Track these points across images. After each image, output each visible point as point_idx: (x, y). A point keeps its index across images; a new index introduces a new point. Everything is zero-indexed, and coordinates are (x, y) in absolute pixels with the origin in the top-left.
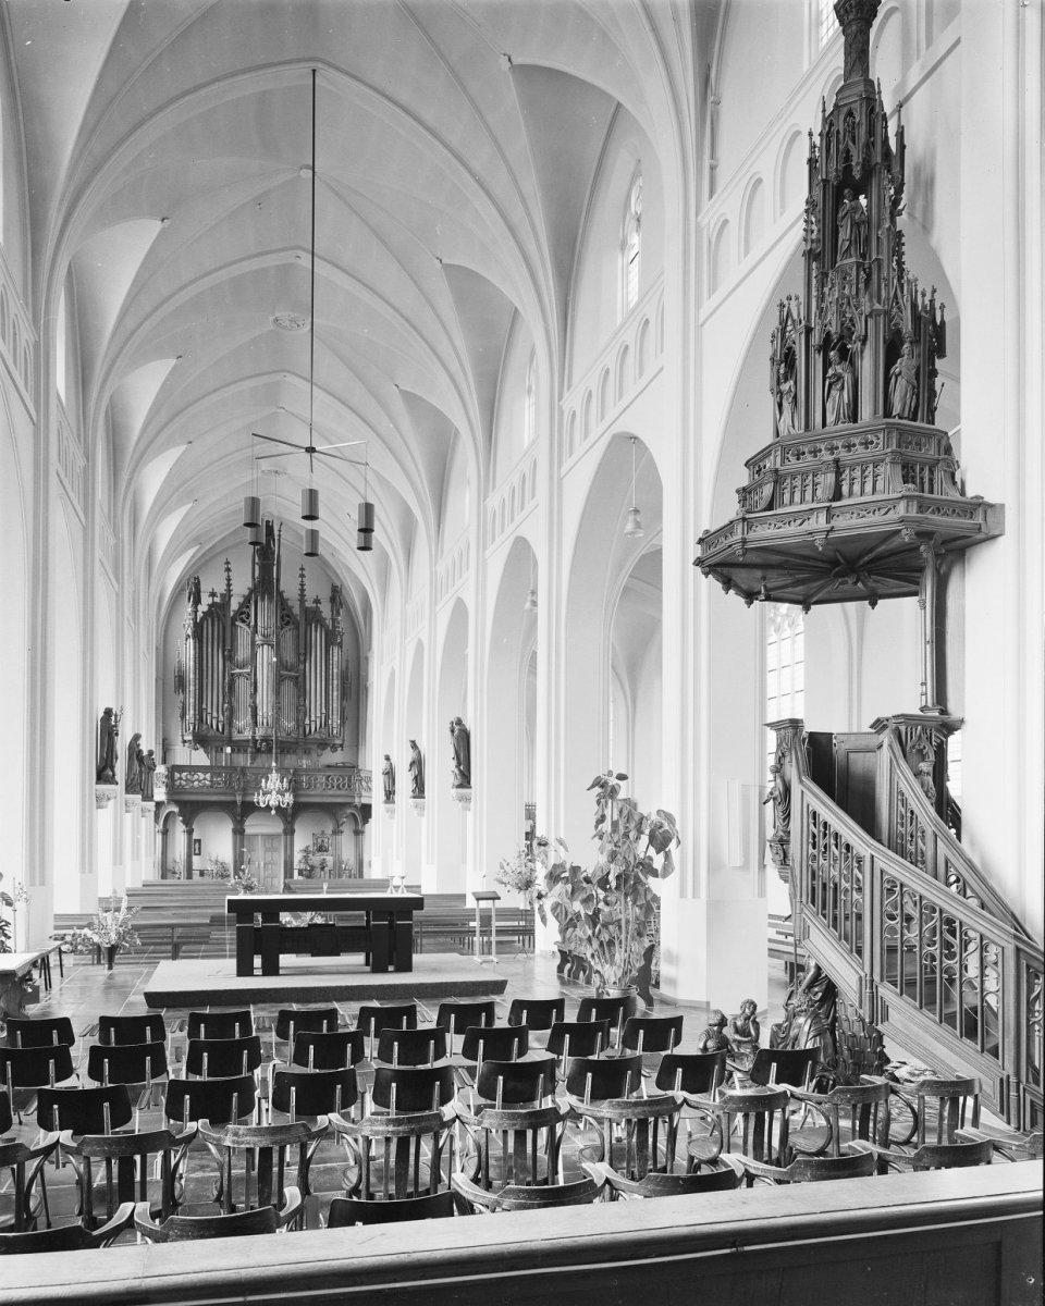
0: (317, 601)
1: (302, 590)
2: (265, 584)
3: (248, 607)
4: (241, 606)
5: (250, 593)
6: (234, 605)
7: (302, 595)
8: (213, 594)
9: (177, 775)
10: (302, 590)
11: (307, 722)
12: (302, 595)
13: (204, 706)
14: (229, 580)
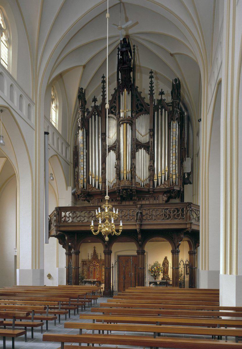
0: (162, 93)
1: (151, 87)
3: (114, 102)
7: (151, 90)
9: (63, 214)
10: (151, 87)
12: (151, 90)
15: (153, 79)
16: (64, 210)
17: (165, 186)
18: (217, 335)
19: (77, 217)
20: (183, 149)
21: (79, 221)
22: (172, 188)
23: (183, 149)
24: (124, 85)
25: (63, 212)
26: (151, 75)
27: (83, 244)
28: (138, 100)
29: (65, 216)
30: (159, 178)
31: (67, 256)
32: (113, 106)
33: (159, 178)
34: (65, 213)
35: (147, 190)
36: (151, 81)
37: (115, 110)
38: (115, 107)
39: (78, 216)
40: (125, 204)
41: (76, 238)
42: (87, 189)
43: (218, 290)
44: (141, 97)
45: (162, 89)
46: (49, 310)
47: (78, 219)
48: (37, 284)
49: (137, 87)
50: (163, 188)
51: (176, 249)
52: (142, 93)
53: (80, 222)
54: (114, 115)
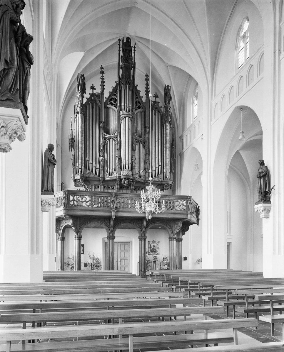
2: (127, 77)
3: (115, 95)
4: (111, 94)
5: (117, 85)
6: (106, 95)
8: (93, 88)
9: (71, 198)
11: (150, 171)
13: (87, 159)
14: (103, 78)
15: (148, 82)
16: (72, 194)
17: (159, 179)
18: (173, 316)
19: (85, 201)
20: (173, 148)
21: (89, 206)
22: (167, 183)
23: (173, 148)
24: (127, 82)
25: (71, 196)
26: (102, 70)
27: (84, 229)
28: (137, 98)
29: (74, 200)
30: (112, 170)
31: (77, 240)
32: (113, 98)
33: (112, 170)
34: (74, 197)
35: (143, 181)
36: (147, 83)
37: (115, 102)
38: (116, 100)
39: (181, 204)
40: (122, 192)
41: (78, 223)
42: (85, 174)
43: (262, 273)
44: (139, 95)
45: (93, 84)
46: (201, 292)
47: (181, 207)
48: (223, 266)
49: (137, 85)
50: (157, 180)
51: (173, 236)
52: (105, 86)
53: (90, 206)
54: (115, 106)
